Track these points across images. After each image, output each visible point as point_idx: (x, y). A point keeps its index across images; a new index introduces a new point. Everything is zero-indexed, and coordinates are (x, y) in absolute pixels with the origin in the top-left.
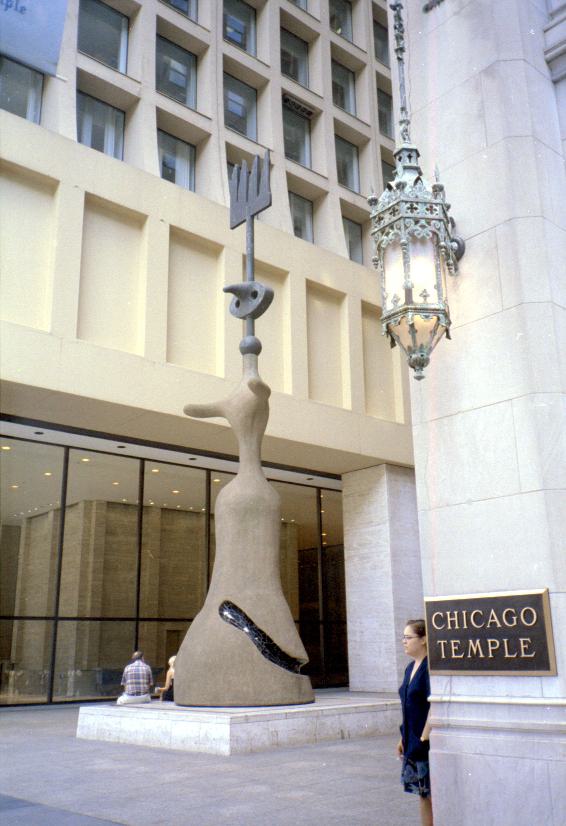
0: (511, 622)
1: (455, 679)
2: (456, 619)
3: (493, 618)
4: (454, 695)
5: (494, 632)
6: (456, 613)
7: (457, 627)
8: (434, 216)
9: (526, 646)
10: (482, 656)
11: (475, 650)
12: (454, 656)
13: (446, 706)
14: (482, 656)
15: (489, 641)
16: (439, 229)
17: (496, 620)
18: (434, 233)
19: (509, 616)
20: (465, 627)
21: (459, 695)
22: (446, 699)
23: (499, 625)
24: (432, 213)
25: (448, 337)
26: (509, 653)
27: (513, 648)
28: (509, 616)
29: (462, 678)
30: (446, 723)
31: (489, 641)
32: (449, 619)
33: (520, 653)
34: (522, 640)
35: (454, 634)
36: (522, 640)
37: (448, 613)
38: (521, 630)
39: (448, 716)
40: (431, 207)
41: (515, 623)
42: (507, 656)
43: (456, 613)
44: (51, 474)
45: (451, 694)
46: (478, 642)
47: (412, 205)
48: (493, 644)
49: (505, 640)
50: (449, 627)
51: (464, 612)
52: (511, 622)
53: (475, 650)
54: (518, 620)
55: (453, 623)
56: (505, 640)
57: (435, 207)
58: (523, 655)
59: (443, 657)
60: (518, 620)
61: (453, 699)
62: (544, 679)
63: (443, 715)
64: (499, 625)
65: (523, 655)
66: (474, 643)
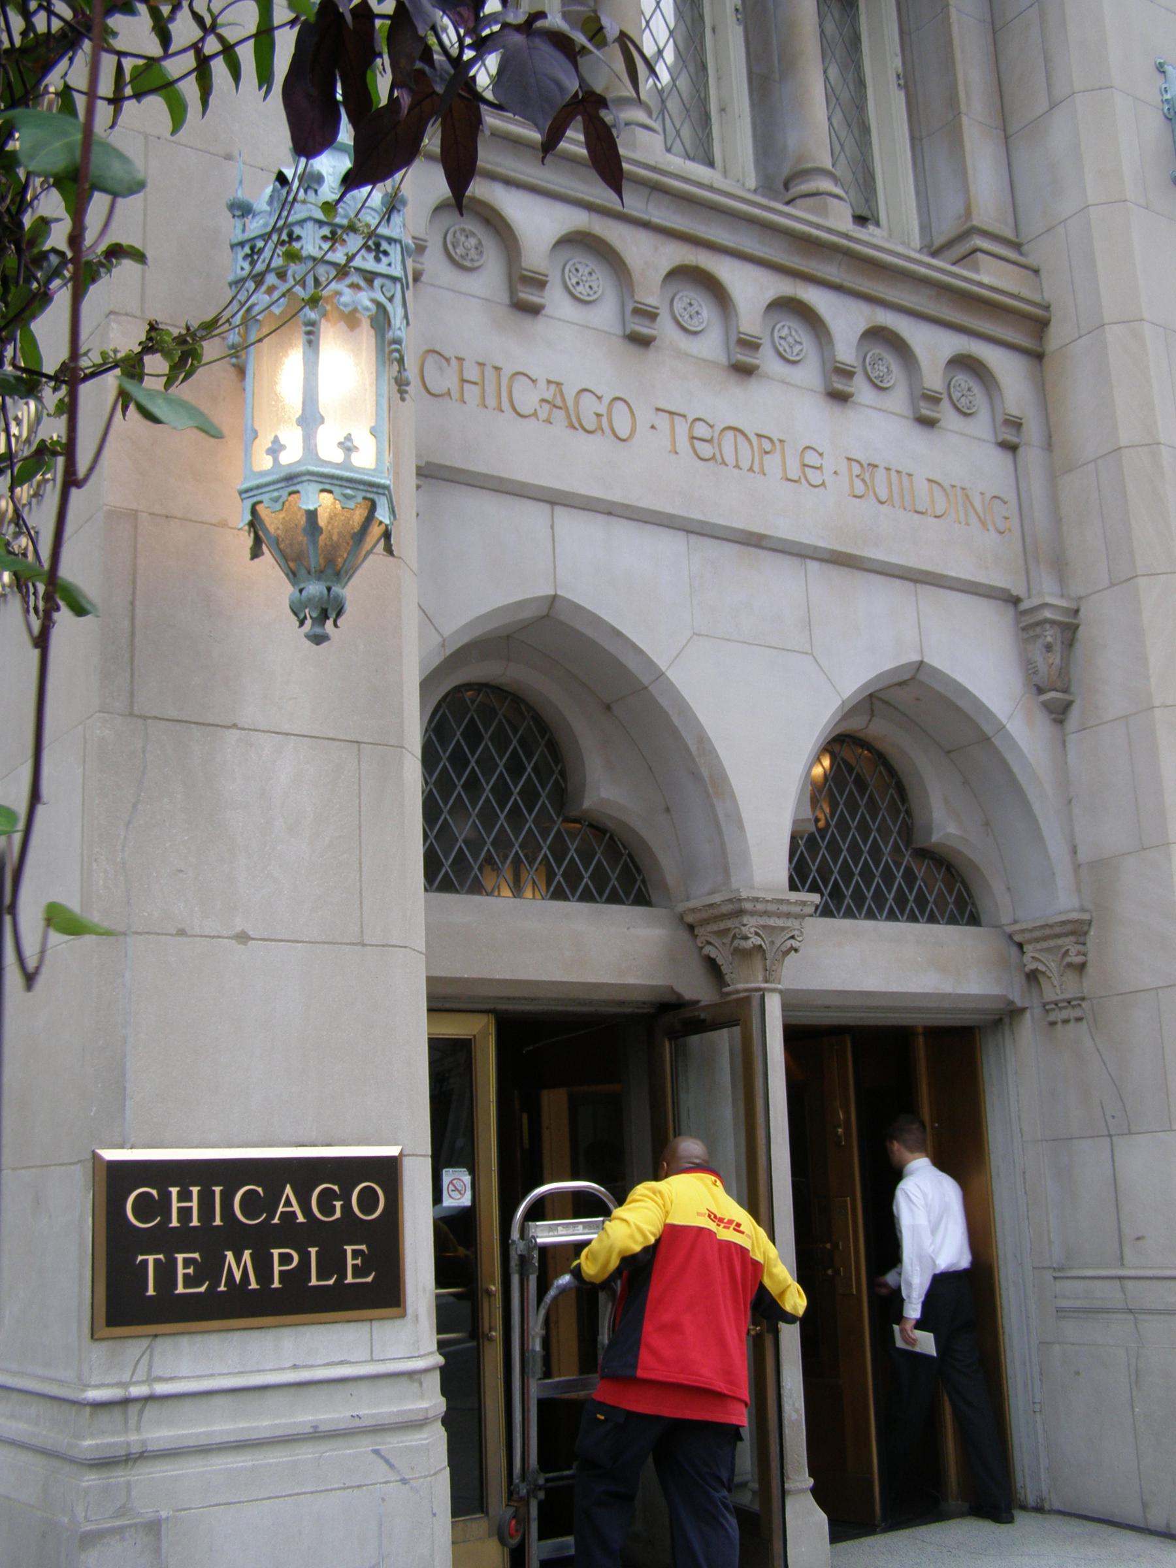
0: (327, 1209)
1: (162, 1345)
2: (194, 1204)
3: (288, 1203)
4: (160, 1379)
5: (289, 1232)
6: (195, 1190)
7: (195, 1222)
8: (382, 268)
9: (358, 1262)
10: (254, 1285)
11: (238, 1276)
12: (180, 1290)
13: (133, 1410)
14: (254, 1285)
15: (276, 1252)
16: (391, 299)
17: (296, 1208)
18: (379, 305)
19: (326, 1202)
20: (218, 1222)
21: (171, 1379)
22: (136, 1391)
23: (301, 1219)
24: (378, 260)
25: (389, 550)
26: (319, 1278)
27: (332, 1263)
28: (326, 1202)
29: (184, 1341)
30: (135, 1449)
31: (276, 1252)
32: (175, 1205)
33: (344, 1276)
34: (349, 1249)
35: (184, 1238)
36: (349, 1249)
37: (174, 1191)
38: (350, 1228)
39: (138, 1429)
40: (378, 245)
41: (338, 1214)
42: (314, 1282)
43: (195, 1190)
44: (473, 379)
45: (151, 1379)
46: (247, 1254)
47: (252, 248)
48: (285, 1259)
49: (313, 1251)
50: (175, 1223)
51: (218, 1190)
52: (327, 1209)
53: (238, 1276)
54: (347, 1208)
55: (185, 1213)
56: (313, 1251)
57: (385, 246)
58: (350, 1279)
59: (151, 1292)
60: (347, 1208)
61: (161, 1388)
62: (376, 1324)
63: (126, 1430)
64: (301, 1219)
65: (350, 1279)
66: (238, 1260)
